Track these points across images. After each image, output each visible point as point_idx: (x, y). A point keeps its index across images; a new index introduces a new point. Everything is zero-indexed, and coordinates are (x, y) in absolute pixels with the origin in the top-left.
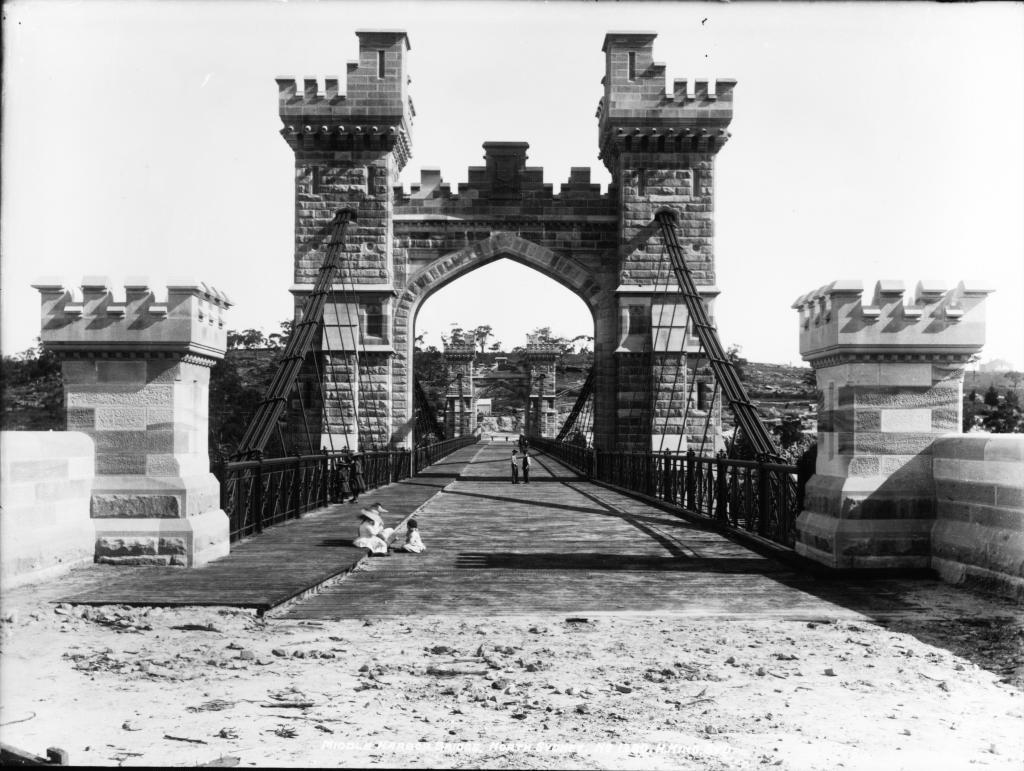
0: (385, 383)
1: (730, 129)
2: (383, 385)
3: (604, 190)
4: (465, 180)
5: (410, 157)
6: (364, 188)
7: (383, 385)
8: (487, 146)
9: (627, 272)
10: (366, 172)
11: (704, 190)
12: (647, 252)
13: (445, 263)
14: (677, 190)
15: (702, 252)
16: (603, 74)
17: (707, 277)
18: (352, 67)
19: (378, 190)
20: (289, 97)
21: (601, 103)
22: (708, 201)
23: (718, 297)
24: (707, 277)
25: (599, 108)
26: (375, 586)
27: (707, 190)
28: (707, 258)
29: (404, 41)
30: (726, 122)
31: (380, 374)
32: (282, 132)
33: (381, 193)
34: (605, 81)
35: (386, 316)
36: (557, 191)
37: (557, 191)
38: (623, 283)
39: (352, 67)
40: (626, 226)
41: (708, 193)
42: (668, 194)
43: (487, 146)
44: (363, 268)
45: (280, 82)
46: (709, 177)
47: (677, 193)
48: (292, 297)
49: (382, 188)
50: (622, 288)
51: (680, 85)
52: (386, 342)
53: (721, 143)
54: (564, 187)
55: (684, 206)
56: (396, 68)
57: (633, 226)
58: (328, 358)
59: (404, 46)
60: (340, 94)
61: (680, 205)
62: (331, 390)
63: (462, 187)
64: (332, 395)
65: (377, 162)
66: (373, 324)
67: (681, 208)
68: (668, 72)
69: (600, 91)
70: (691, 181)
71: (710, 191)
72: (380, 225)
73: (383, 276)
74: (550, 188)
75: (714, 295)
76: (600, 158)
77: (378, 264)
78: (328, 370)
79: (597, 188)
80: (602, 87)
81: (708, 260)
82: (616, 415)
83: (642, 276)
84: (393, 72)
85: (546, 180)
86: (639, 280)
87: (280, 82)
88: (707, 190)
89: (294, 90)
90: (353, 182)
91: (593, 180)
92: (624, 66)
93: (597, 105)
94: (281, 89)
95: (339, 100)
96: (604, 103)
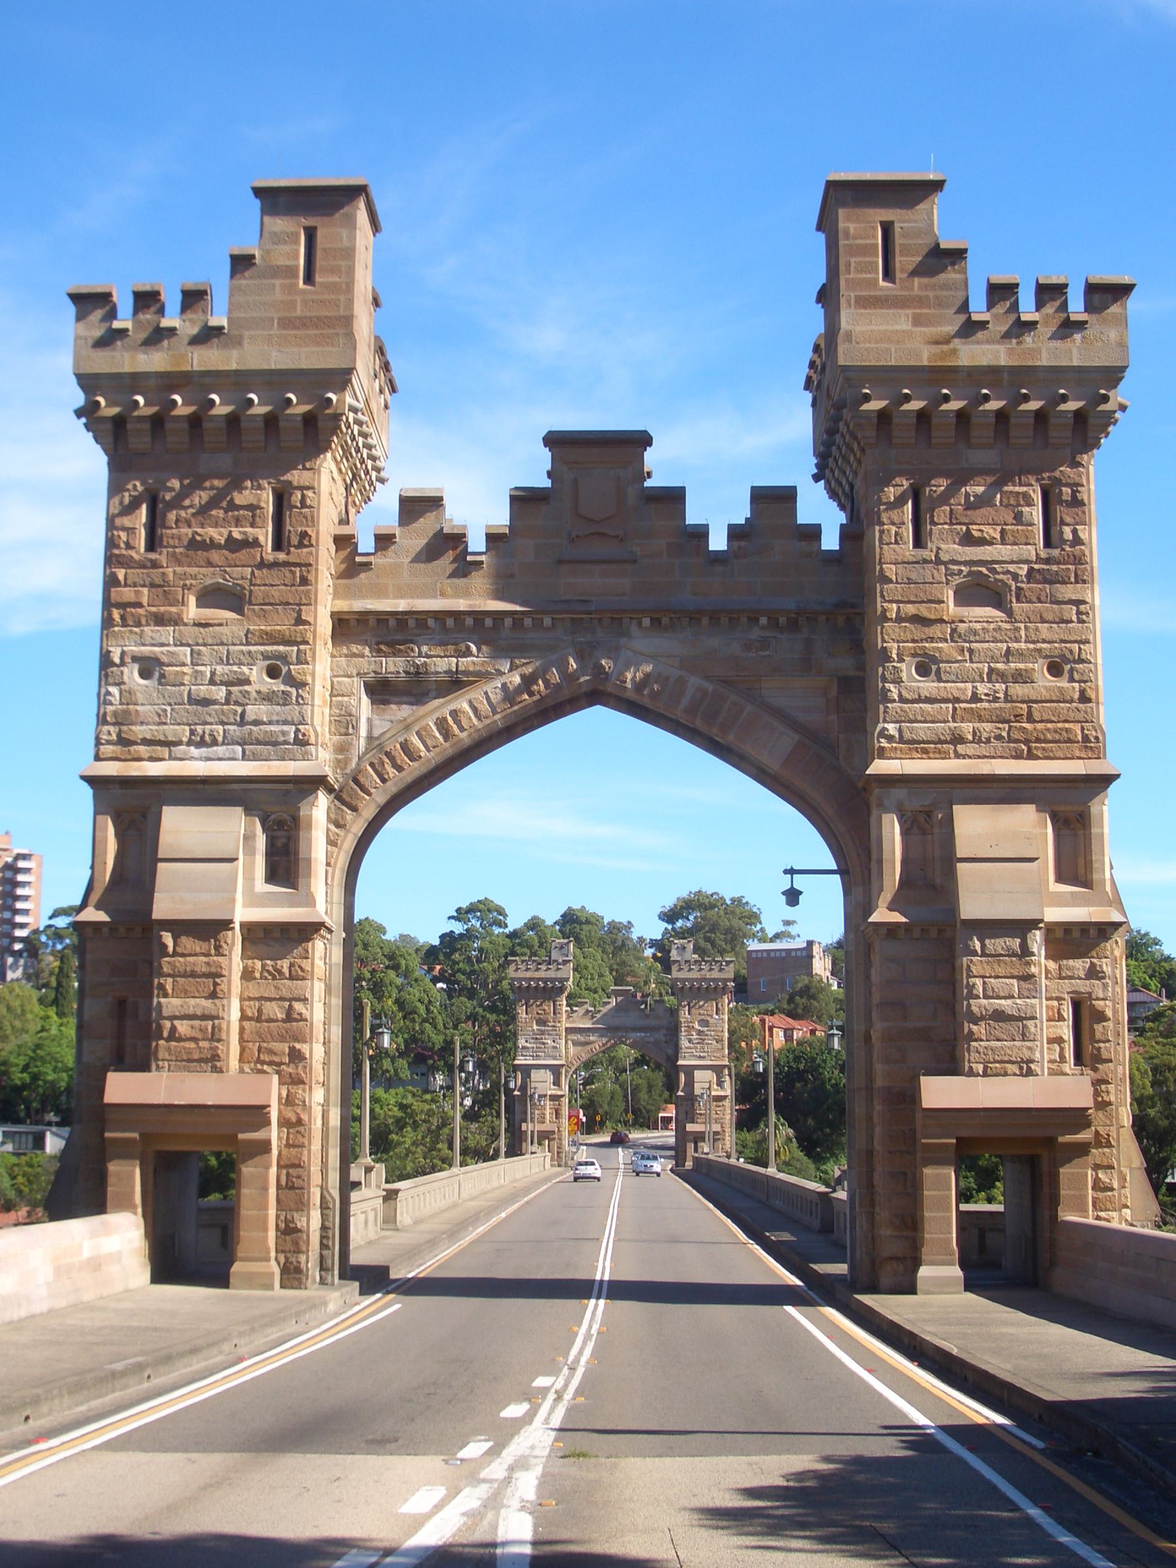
0: (304, 1000)
1: (1119, 395)
2: (298, 1006)
3: (830, 541)
4: (501, 517)
5: (382, 481)
6: (265, 535)
7: (298, 1006)
8: (554, 440)
9: (892, 729)
10: (267, 499)
11: (1068, 533)
12: (940, 680)
13: (454, 714)
14: (1003, 532)
15: (1072, 680)
16: (822, 279)
17: (1086, 739)
18: (241, 263)
19: (295, 540)
20: (98, 333)
21: (816, 349)
22: (1079, 560)
23: (1114, 787)
24: (1086, 739)
25: (812, 365)
26: (481, 1229)
27: (1075, 532)
28: (1082, 692)
29: (362, 205)
30: (1113, 375)
31: (291, 978)
32: (79, 413)
33: (301, 545)
34: (827, 296)
35: (316, 859)
36: (718, 542)
37: (718, 542)
38: (882, 754)
39: (241, 263)
40: (884, 618)
41: (1077, 541)
42: (982, 542)
43: (554, 440)
44: (257, 723)
45: (77, 298)
46: (1077, 503)
47: (1003, 542)
48: (87, 792)
49: (304, 535)
50: (879, 767)
51: (1001, 292)
52: (1087, 1217)
53: (1108, 419)
54: (735, 532)
55: (1023, 570)
56: (343, 263)
57: (899, 619)
58: (168, 939)
59: (362, 216)
60: (214, 322)
61: (1012, 568)
62: (172, 1018)
63: (493, 538)
64: (173, 1029)
65: (296, 476)
66: (947, 1192)
67: (1015, 577)
68: (972, 261)
69: (814, 321)
70: (1036, 514)
71: (1083, 536)
72: (299, 621)
73: (301, 741)
74: (701, 533)
75: (1107, 780)
76: (816, 478)
77: (292, 711)
78: (166, 969)
79: (813, 532)
80: (819, 312)
81: (1084, 698)
82: (912, 1095)
83: (922, 736)
84: (334, 270)
85: (693, 517)
86: (919, 747)
87: (77, 298)
88: (1075, 532)
89: (112, 314)
90: (238, 522)
91: (805, 514)
92: (870, 250)
93: (809, 354)
94: (80, 317)
95: (208, 335)
96: (826, 347)
